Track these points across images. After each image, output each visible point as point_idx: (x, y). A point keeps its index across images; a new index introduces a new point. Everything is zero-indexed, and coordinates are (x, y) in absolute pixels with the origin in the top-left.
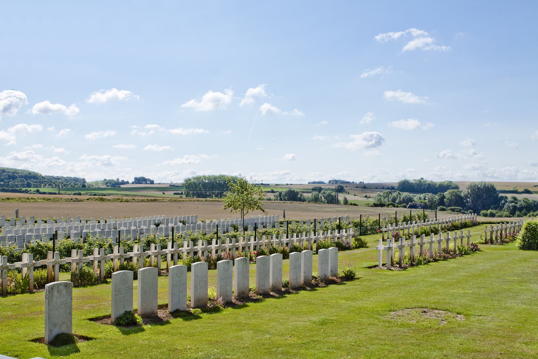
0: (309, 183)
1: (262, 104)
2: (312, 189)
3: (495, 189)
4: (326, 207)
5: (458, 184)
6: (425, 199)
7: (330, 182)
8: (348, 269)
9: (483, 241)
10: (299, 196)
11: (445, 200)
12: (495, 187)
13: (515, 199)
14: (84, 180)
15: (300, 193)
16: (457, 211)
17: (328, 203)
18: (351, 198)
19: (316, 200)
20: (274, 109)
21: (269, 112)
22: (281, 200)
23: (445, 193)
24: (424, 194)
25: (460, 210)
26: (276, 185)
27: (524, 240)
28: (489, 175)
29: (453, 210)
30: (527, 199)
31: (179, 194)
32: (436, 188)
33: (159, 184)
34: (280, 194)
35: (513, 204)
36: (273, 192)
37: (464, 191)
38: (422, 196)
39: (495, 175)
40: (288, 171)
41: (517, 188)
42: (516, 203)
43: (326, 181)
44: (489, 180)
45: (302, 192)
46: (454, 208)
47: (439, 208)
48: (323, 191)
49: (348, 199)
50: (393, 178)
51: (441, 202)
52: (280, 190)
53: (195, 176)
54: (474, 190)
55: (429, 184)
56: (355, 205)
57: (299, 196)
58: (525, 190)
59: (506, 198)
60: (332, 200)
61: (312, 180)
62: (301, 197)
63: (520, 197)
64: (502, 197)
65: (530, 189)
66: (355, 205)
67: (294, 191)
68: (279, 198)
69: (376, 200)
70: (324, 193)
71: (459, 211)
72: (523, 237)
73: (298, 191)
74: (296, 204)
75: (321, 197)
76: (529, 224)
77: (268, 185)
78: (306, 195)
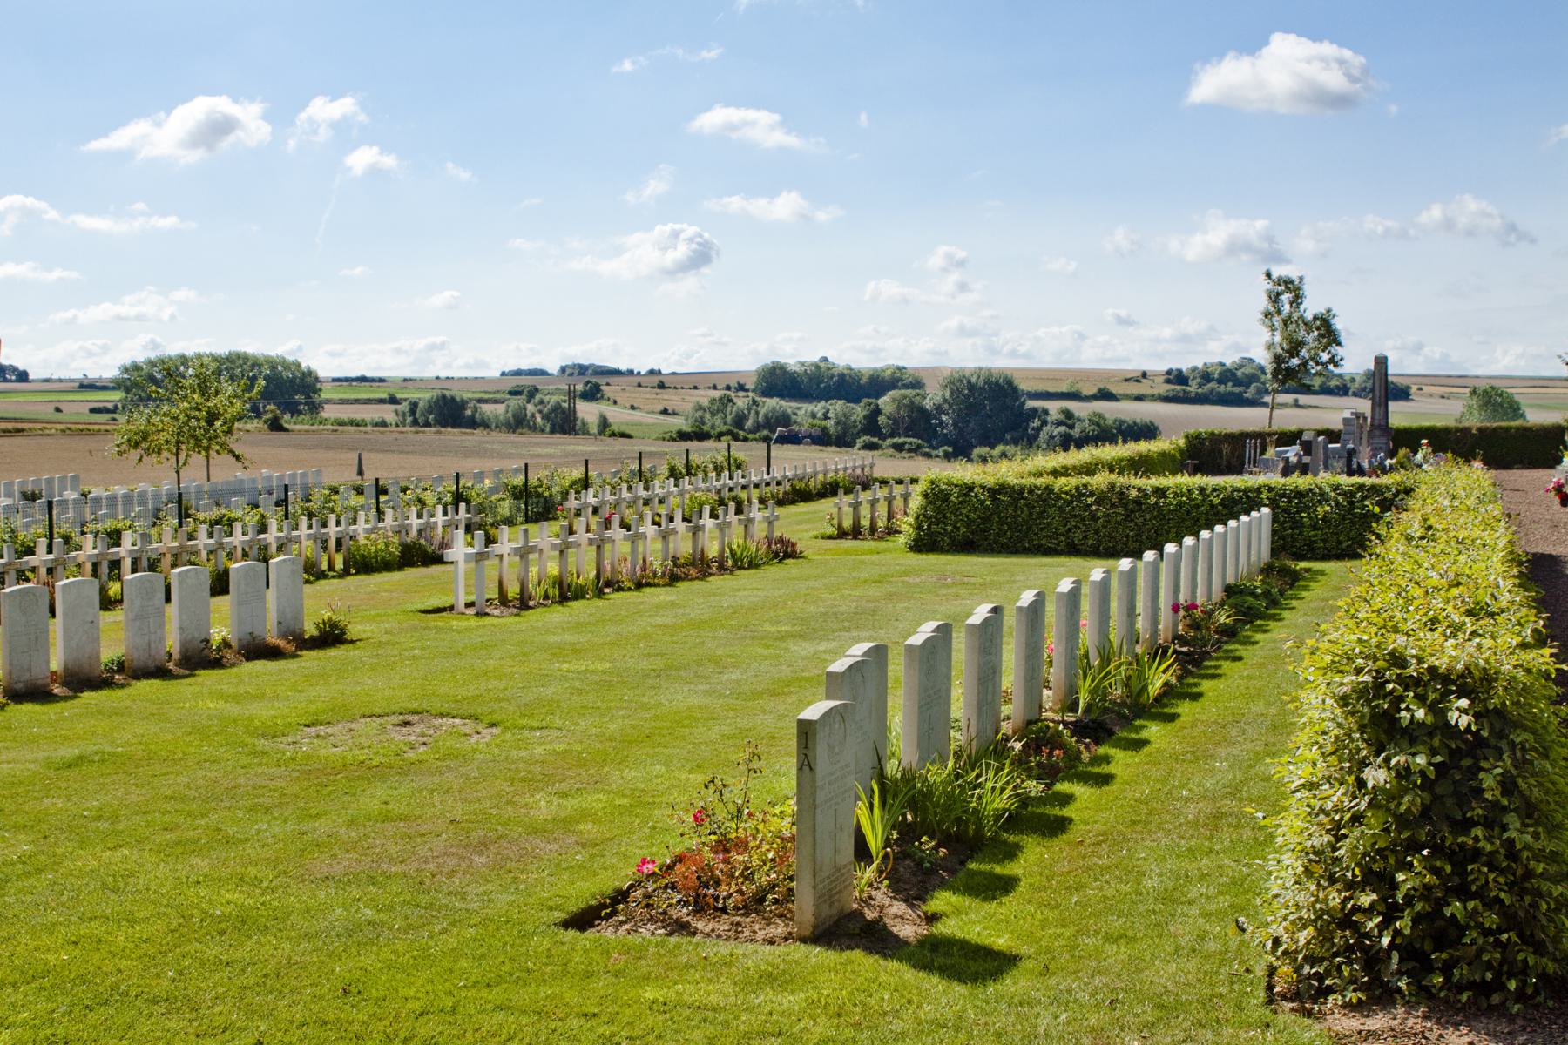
0: (503, 374)
1: (355, 147)
2: (511, 393)
3: (1014, 390)
4: (538, 444)
5: (922, 374)
6: (826, 417)
7: (563, 370)
8: (327, 615)
9: (833, 531)
10: (469, 412)
11: (882, 419)
12: (1016, 382)
13: (1068, 414)
14: (1180, 371)
15: (471, 405)
16: (910, 451)
17: (553, 432)
18: (618, 416)
19: (518, 423)
20: (389, 161)
21: (374, 172)
22: (415, 423)
23: (881, 401)
24: (823, 403)
25: (919, 447)
26: (405, 380)
27: (919, 528)
28: (1005, 350)
29: (899, 448)
30: (1100, 416)
31: (107, 411)
32: (860, 387)
33: (46, 381)
34: (414, 406)
35: (1062, 429)
36: (393, 400)
37: (933, 396)
38: (818, 407)
39: (1022, 349)
40: (439, 340)
41: (1080, 385)
42: (1072, 427)
43: (553, 368)
44: (1000, 362)
45: (481, 401)
46: (901, 440)
47: (860, 441)
48: (538, 397)
49: (610, 421)
50: (744, 355)
51: (871, 425)
52: (414, 396)
53: (153, 356)
54: (959, 391)
55: (842, 376)
56: (624, 435)
57: (469, 412)
58: (1100, 390)
59: (1046, 412)
60: (564, 423)
61: (512, 366)
62: (473, 416)
63: (1080, 409)
64: (1034, 411)
65: (1114, 390)
66: (624, 435)
67: (453, 399)
68: (409, 420)
69: (691, 421)
70: (541, 402)
71: (916, 450)
72: (917, 518)
73: (466, 396)
74: (453, 435)
75: (533, 416)
76: (932, 482)
77: (381, 380)
78: (487, 409)
